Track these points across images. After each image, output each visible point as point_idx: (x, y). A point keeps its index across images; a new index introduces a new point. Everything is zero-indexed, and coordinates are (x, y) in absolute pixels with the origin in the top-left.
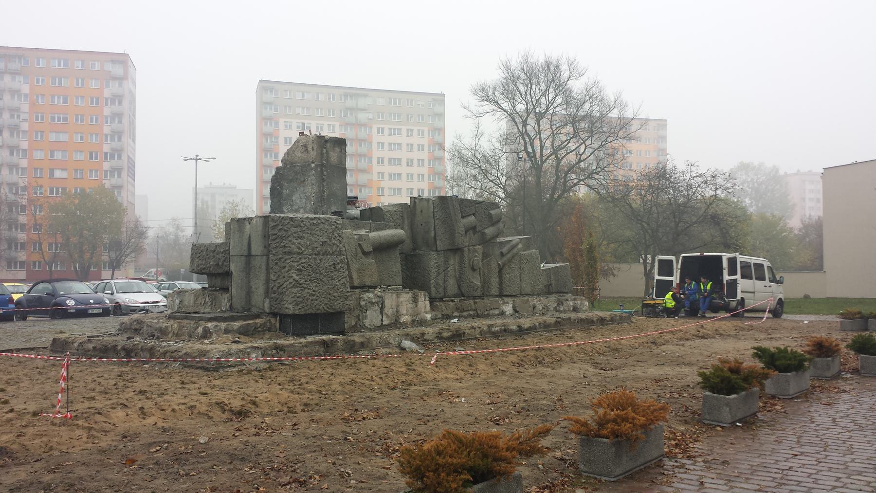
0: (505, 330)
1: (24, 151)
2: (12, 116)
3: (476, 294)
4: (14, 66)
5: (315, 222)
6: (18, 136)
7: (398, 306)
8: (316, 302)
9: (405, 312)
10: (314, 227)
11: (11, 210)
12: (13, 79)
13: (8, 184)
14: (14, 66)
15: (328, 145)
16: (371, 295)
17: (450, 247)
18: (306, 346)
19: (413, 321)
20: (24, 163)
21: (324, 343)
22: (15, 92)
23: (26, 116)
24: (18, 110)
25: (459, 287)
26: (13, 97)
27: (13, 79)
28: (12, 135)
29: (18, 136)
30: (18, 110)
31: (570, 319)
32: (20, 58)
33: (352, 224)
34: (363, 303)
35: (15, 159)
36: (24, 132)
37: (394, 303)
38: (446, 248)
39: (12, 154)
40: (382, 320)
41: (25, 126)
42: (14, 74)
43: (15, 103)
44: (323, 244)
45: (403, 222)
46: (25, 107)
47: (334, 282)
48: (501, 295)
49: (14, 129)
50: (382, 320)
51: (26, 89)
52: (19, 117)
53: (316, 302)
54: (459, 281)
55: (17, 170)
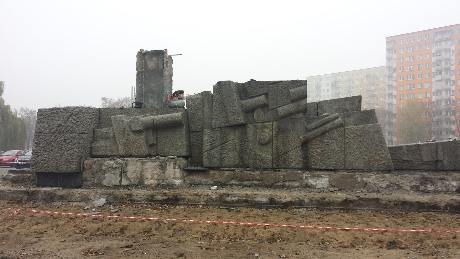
0: (246, 201)
1: (453, 81)
2: (446, 63)
3: (266, 166)
4: (446, 36)
5: (54, 111)
6: (450, 74)
7: (142, 171)
8: (46, 165)
9: (150, 176)
10: (54, 115)
11: (447, 114)
12: (446, 43)
13: (446, 100)
14: (446, 36)
15: (146, 57)
16: (112, 162)
17: (227, 125)
18: (13, 193)
19: (159, 184)
20: (453, 88)
21: (27, 193)
22: (447, 50)
23: (454, 62)
24: (449, 59)
25: (241, 158)
26: (446, 53)
27: (446, 43)
28: (447, 73)
29: (450, 74)
30: (449, 59)
31: (378, 200)
32: (449, 31)
33: (139, 111)
34: (104, 168)
35: (448, 86)
36: (453, 71)
37: (138, 170)
38: (223, 125)
39: (447, 84)
40: (121, 181)
41: (453, 68)
42: (446, 40)
43: (448, 56)
44: (60, 125)
45: (203, 106)
46: (453, 57)
47: (63, 152)
48: (307, 167)
49: (448, 70)
50: (121, 181)
51: (453, 48)
52: (450, 63)
53: (46, 165)
54: (241, 153)
55: (450, 91)
